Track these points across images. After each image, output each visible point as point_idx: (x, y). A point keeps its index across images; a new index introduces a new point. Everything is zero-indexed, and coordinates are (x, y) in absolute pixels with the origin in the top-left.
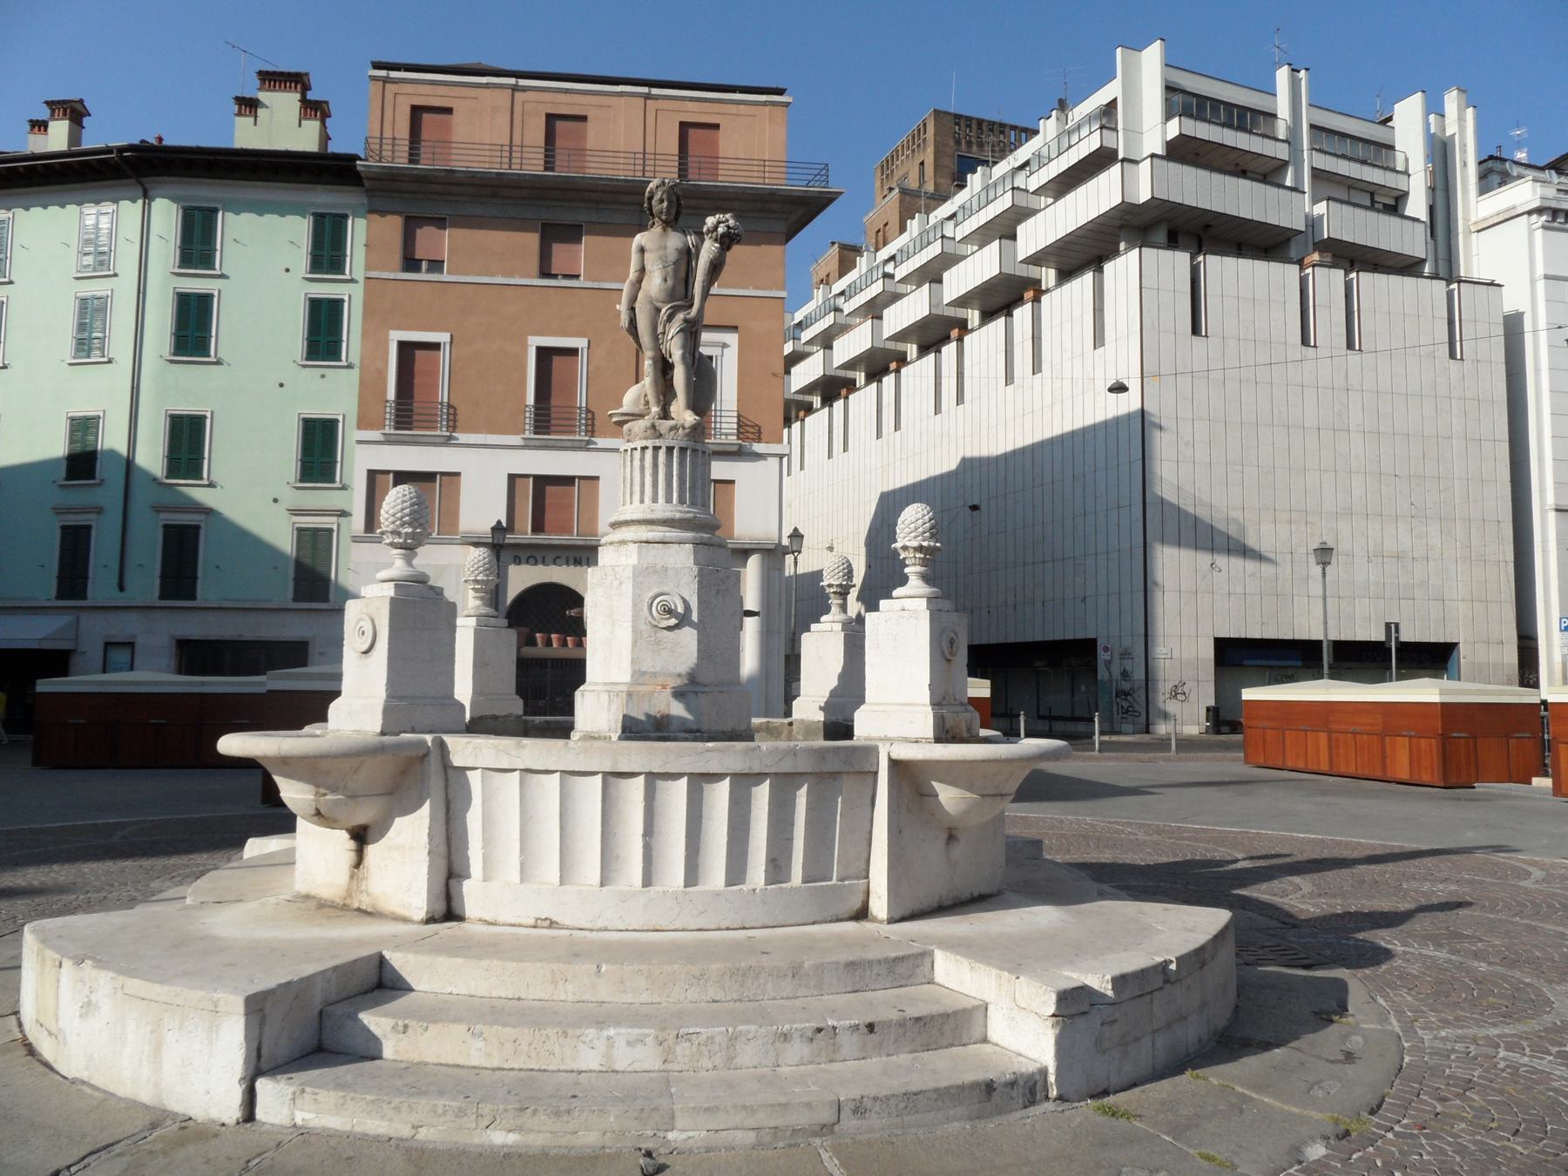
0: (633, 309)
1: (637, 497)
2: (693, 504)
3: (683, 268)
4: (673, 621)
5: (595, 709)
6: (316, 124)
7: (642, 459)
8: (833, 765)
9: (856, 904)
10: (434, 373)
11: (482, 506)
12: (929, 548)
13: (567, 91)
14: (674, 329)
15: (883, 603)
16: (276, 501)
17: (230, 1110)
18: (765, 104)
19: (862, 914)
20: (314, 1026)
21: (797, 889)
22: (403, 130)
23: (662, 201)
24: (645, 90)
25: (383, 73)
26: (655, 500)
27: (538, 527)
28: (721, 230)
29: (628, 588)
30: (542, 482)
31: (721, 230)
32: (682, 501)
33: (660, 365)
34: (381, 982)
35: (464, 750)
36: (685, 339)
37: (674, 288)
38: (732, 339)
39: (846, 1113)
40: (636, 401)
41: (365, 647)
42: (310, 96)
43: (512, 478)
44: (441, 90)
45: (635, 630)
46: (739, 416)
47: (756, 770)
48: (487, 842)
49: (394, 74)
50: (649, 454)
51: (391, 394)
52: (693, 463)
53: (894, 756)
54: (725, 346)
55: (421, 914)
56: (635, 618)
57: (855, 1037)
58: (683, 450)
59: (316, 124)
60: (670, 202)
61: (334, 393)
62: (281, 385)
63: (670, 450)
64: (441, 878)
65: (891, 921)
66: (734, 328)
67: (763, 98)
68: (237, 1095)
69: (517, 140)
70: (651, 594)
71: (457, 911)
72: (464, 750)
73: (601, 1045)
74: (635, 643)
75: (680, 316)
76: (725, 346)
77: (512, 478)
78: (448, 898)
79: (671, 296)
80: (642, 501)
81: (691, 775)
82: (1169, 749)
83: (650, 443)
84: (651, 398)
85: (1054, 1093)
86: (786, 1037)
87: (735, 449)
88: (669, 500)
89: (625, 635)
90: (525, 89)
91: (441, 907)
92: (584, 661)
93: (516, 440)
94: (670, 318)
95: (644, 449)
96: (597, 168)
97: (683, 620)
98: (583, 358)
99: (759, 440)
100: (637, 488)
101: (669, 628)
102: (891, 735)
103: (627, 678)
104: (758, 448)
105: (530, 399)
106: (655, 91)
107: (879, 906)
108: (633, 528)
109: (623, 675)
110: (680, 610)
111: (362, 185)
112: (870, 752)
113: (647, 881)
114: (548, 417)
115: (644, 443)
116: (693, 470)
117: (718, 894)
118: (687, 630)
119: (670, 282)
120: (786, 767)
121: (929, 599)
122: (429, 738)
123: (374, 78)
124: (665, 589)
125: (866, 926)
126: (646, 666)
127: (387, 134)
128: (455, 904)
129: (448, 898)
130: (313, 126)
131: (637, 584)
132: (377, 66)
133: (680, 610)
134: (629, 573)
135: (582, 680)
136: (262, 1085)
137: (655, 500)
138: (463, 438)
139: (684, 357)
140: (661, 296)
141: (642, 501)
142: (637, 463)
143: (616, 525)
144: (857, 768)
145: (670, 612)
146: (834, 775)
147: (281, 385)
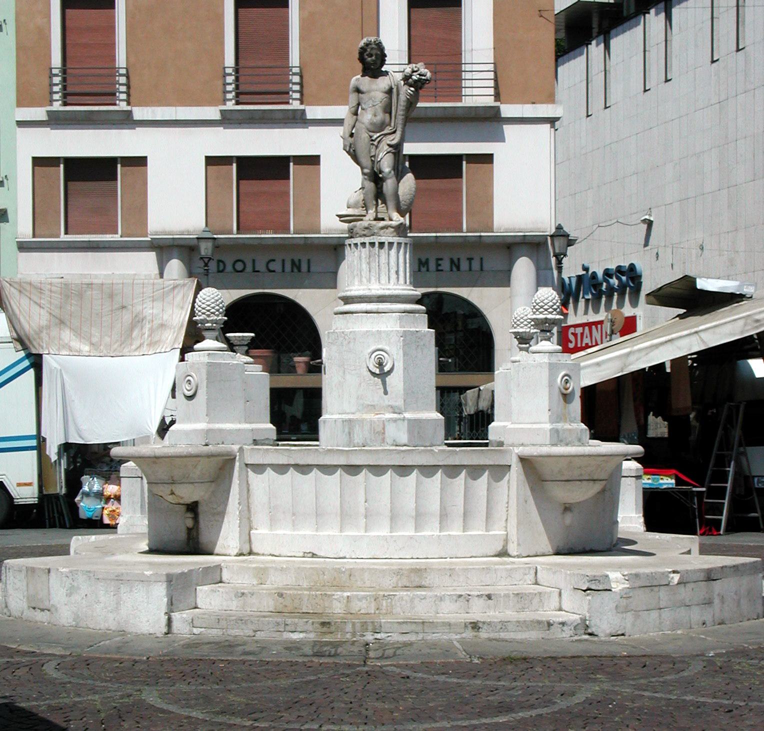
30: (255, 169)
71: (205, 538)
93: (212, 113)
110: (386, 369)
133: (386, 369)
145: (380, 365)
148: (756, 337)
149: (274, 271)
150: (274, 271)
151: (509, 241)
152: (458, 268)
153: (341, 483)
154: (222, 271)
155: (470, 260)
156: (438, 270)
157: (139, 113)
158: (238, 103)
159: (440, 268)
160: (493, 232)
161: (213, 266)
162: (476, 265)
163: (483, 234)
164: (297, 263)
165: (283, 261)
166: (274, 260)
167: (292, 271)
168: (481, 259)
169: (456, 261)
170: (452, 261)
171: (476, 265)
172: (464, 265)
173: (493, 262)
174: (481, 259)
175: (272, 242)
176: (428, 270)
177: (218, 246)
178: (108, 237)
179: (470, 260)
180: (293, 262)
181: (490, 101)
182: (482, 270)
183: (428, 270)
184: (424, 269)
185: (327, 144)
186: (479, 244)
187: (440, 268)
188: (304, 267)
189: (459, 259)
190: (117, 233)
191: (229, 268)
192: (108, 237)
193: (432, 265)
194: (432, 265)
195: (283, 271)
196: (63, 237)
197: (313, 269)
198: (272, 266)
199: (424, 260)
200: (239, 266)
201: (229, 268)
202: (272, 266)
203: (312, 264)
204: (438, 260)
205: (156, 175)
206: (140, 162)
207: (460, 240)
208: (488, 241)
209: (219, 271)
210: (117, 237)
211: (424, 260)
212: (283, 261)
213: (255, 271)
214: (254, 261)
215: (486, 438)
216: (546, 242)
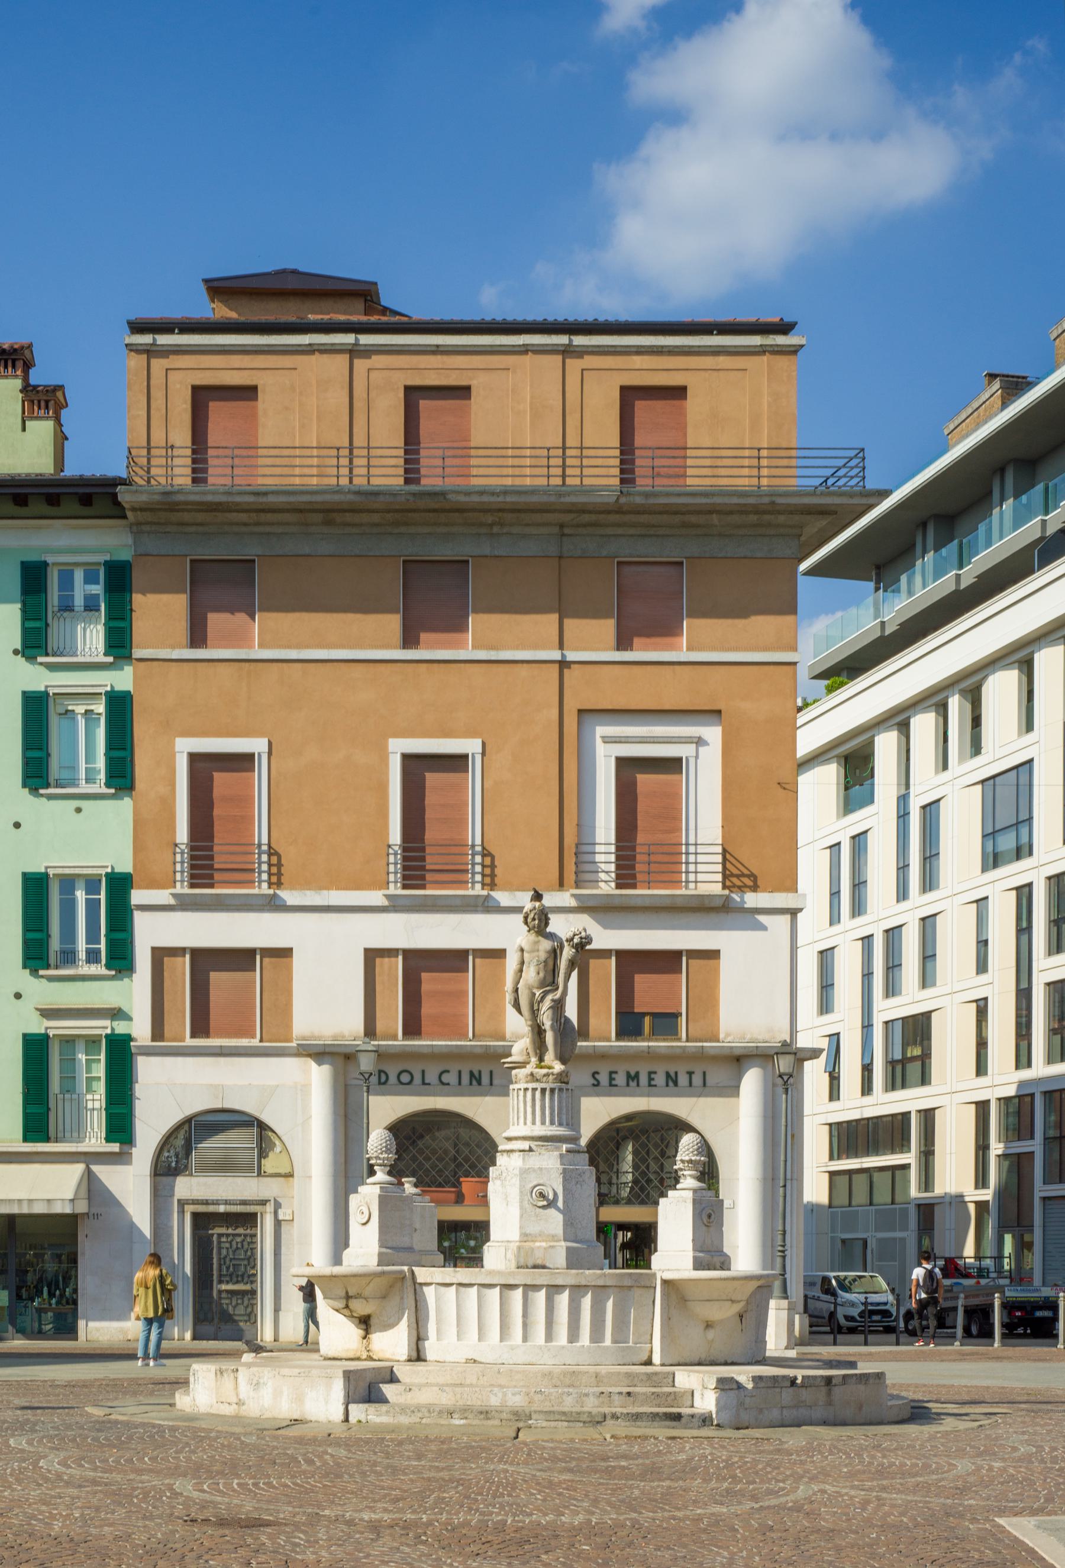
0: (516, 990)
1: (522, 1120)
2: (560, 1124)
3: (551, 963)
4: (545, 1203)
5: (497, 1256)
6: (49, 425)
7: (525, 1096)
8: (627, 1282)
9: (645, 1358)
10: (245, 801)
11: (328, 999)
12: (695, 1161)
13: (437, 350)
14: (547, 1003)
15: (670, 1193)
16: (18, 996)
17: (339, 1416)
18: (761, 351)
19: (649, 1362)
20: (367, 1386)
21: (608, 1347)
22: (182, 437)
23: (534, 919)
24: (562, 339)
25: (146, 339)
26: (534, 1123)
27: (412, 1028)
28: (575, 941)
29: (516, 1181)
30: (419, 962)
31: (575, 941)
32: (552, 1123)
33: (536, 1030)
34: (393, 1379)
35: (422, 1274)
36: (553, 1014)
37: (545, 978)
38: (713, 734)
39: (608, 1418)
40: (521, 1053)
41: (364, 1221)
42: (36, 377)
43: (372, 956)
44: (236, 360)
45: (521, 1207)
46: (725, 852)
47: (583, 1283)
48: (439, 1322)
49: (163, 340)
50: (529, 1094)
51: (182, 835)
52: (560, 1097)
53: (664, 1277)
54: (699, 742)
55: (405, 1357)
56: (521, 1201)
57: (622, 1398)
58: (552, 1090)
59: (49, 425)
60: (540, 920)
61: (91, 836)
62: (17, 825)
63: (543, 1091)
64: (415, 1339)
65: (663, 1365)
66: (714, 714)
67: (756, 340)
68: (341, 1409)
69: (359, 440)
70: (532, 1185)
71: (423, 1357)
72: (422, 1274)
73: (500, 1395)
74: (521, 1216)
75: (550, 997)
76: (699, 742)
77: (372, 956)
78: (418, 1350)
79: (542, 984)
80: (525, 1124)
81: (548, 1286)
82: (1008, 1307)
83: (531, 1086)
84: (530, 1051)
85: (715, 1423)
86: (587, 1395)
87: (719, 903)
88: (543, 1123)
89: (515, 1211)
90: (368, 352)
91: (414, 1355)
92: (656, 1223)
93: (376, 897)
94: (543, 999)
95: (526, 1089)
96: (486, 476)
97: (551, 1204)
98: (476, 765)
99: (755, 888)
100: (522, 1115)
101: (543, 1207)
102: (663, 1268)
103: (517, 1238)
104: (751, 900)
105: (395, 836)
106: (579, 340)
107: (657, 1359)
108: (519, 1142)
109: (515, 1235)
110: (551, 1197)
111: (125, 517)
112: (654, 1275)
113: (525, 1339)
114: (422, 863)
115: (526, 1086)
116: (560, 1102)
117: (563, 1347)
118: (552, 1212)
119: (542, 975)
120: (600, 1283)
121: (695, 1191)
122: (406, 1268)
123: (131, 348)
124: (541, 1182)
125: (649, 1369)
126: (533, 1229)
127: (158, 437)
128: (421, 1354)
129: (418, 1350)
130: (42, 429)
131: (522, 1180)
132: (138, 327)
133: (551, 1197)
134: (517, 1172)
135: (488, 1239)
136: (352, 1407)
137: (534, 1123)
138: (290, 897)
139: (552, 1026)
140: (536, 984)
141: (525, 1124)
142: (521, 1098)
143: (509, 1139)
144: (643, 1284)
145: (542, 1195)
146: (630, 1287)
147: (17, 825)
148: (384, 1250)
149: (448, 1084)
150: (448, 1084)
151: (738, 1052)
152: (676, 1084)
153: (458, 1326)
154: (385, 1083)
155: (690, 1074)
156: (650, 1085)
157: (290, 897)
158: (405, 887)
159: (653, 1083)
160: (718, 1041)
161: (374, 1079)
162: (697, 1080)
163: (705, 1044)
164: (477, 1075)
165: (460, 1072)
166: (448, 1071)
167: (471, 1084)
168: (704, 1073)
169: (477, 1075)
170: (668, 1075)
171: (697, 1080)
172: (683, 1080)
173: (717, 1075)
174: (704, 1073)
175: (444, 1050)
176: (638, 1085)
177: (381, 1055)
178: (244, 1042)
179: (690, 1074)
180: (472, 1074)
181: (717, 889)
182: (704, 1084)
183: (638, 1085)
184: (633, 1084)
185: (507, 933)
186: (701, 1056)
187: (653, 1083)
188: (485, 1080)
189: (676, 1073)
190: (253, 1036)
191: (393, 1079)
192: (244, 1042)
193: (644, 1079)
194: (644, 1079)
195: (460, 1084)
196: (189, 1041)
197: (495, 1082)
198: (445, 1078)
199: (633, 1074)
200: (405, 1078)
201: (393, 1079)
202: (445, 1078)
203: (707, 1077)
204: (650, 1073)
205: (303, 971)
206: (285, 953)
207: (678, 1051)
208: (712, 1052)
209: (380, 1083)
210: (255, 1042)
211: (633, 1074)
212: (460, 1072)
213: (424, 1083)
214: (423, 1072)
215: (717, 1260)
216: (100, 1041)
